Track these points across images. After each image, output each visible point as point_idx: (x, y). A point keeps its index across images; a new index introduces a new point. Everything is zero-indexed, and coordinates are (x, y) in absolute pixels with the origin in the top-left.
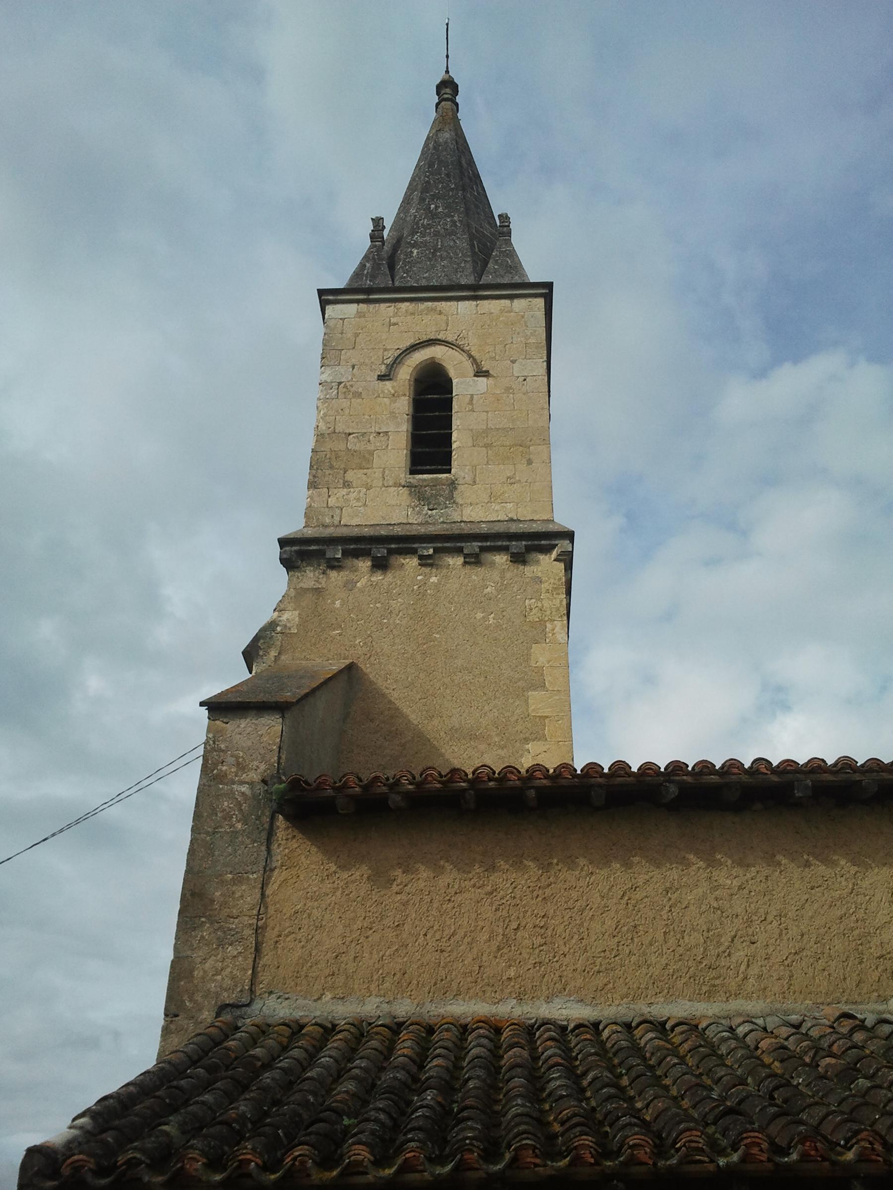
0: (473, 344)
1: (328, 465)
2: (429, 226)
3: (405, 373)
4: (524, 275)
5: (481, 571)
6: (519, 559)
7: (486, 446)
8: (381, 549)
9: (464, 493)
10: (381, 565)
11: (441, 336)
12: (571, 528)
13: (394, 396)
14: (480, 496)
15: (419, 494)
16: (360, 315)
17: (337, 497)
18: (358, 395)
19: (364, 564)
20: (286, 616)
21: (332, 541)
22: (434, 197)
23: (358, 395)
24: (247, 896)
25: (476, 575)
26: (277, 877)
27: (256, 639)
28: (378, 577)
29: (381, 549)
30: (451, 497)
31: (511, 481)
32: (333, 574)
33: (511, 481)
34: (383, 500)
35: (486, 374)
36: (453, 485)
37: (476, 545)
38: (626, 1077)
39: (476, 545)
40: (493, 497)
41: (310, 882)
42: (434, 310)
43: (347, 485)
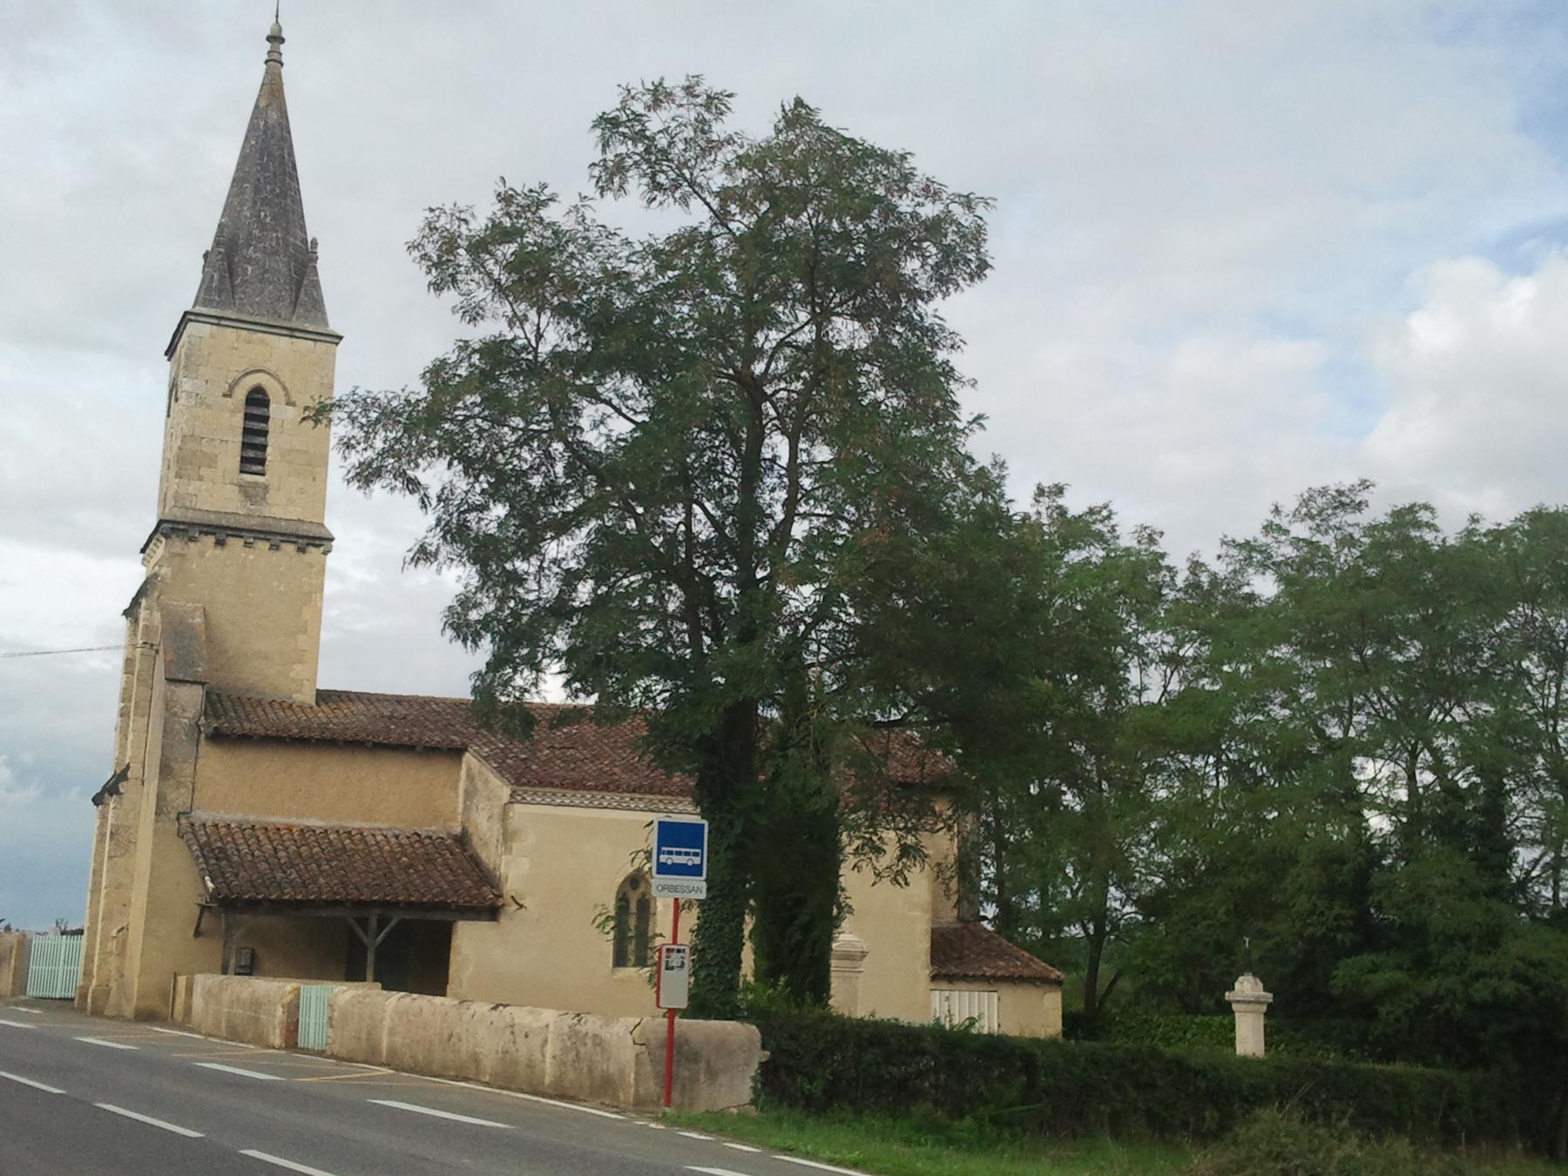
0: (286, 377)
1: (184, 459)
2: (260, 240)
3: (241, 394)
4: (326, 324)
5: (278, 553)
6: (301, 550)
7: (290, 462)
8: (221, 532)
9: (272, 496)
10: (220, 543)
11: (267, 366)
12: (334, 534)
13: (233, 412)
14: (281, 508)
15: (247, 492)
16: (212, 336)
17: (193, 487)
18: (209, 406)
19: (211, 540)
20: (164, 570)
21: (193, 524)
22: (265, 202)
23: (209, 406)
24: (189, 769)
25: (276, 557)
26: (200, 761)
27: (145, 583)
28: (218, 551)
29: (221, 532)
30: (264, 498)
31: (302, 491)
32: (192, 545)
33: (302, 491)
34: (219, 494)
35: (294, 404)
36: (266, 488)
37: (275, 536)
38: (1212, 1002)
39: (275, 536)
40: (291, 501)
41: (215, 765)
42: (261, 341)
43: (201, 478)
